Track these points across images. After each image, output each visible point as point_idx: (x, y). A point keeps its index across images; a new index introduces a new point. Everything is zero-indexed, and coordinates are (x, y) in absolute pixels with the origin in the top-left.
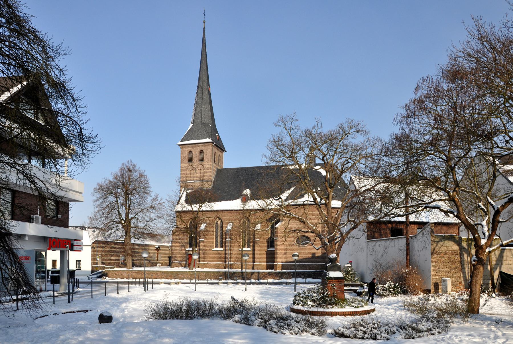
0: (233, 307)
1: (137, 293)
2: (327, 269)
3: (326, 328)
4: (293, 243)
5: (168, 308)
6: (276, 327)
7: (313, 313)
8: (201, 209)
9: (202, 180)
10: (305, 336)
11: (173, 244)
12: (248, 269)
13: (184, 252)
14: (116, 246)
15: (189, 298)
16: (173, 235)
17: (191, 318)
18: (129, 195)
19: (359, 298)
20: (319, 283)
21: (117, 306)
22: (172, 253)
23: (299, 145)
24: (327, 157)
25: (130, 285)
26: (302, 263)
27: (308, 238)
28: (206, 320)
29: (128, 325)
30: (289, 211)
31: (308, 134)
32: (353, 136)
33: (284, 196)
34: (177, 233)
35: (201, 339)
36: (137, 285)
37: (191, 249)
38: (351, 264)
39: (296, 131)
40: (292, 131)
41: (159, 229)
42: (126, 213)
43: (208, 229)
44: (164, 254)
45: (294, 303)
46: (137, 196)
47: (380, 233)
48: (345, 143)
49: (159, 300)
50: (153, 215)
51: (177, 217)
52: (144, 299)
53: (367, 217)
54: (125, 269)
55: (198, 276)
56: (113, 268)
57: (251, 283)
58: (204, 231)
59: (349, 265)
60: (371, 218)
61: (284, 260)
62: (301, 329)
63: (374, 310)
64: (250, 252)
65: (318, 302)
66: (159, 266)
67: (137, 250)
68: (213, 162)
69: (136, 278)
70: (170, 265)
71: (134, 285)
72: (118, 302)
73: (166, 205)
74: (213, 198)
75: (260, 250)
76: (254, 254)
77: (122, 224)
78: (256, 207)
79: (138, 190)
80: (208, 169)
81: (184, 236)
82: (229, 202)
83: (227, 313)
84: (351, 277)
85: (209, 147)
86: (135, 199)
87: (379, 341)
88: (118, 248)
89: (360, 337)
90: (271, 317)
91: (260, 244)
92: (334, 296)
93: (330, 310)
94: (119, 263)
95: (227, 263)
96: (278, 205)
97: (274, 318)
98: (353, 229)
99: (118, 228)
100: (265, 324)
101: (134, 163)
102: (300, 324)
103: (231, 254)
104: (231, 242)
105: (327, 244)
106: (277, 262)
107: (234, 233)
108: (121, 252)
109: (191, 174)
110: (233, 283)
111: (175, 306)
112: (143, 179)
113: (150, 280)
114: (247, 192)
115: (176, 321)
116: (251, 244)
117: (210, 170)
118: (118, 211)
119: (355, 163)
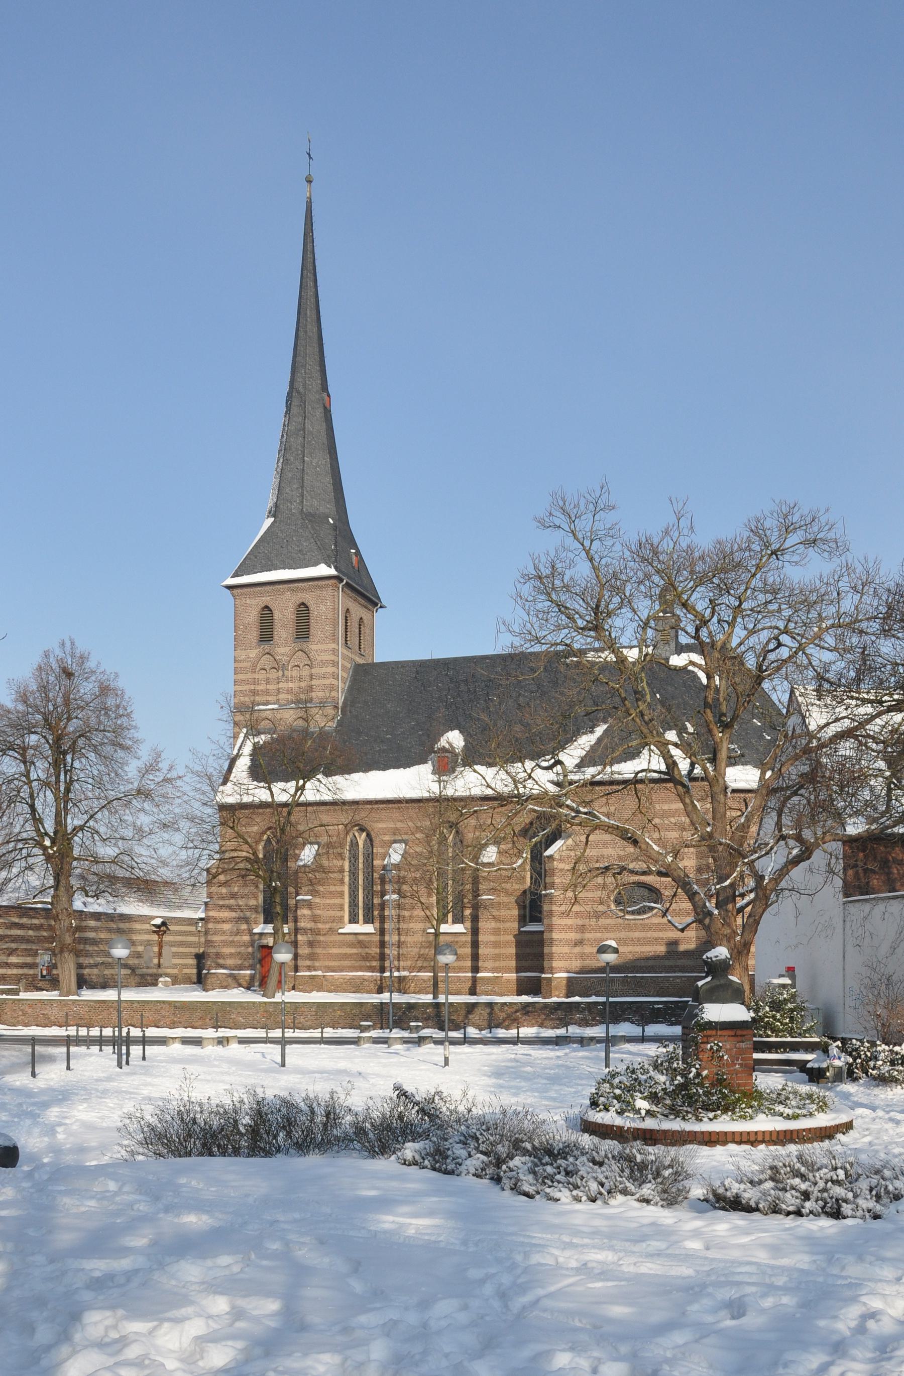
0: (401, 1117)
1: (96, 1076)
2: (700, 997)
3: (686, 1183)
4: (601, 908)
5: (194, 1121)
6: (530, 1178)
7: (650, 1137)
8: (302, 799)
9: (303, 703)
10: (620, 1205)
11: (211, 914)
12: (458, 993)
13: (246, 938)
14: (24, 921)
15: (259, 1091)
16: (209, 883)
17: (268, 1154)
18: (65, 753)
19: (814, 1088)
20: (672, 1039)
21: (34, 1116)
22: (208, 943)
23: (619, 590)
24: (713, 625)
25: (72, 1049)
26: (633, 973)
27: (654, 893)
28: (313, 1160)
29: (66, 1173)
30: (586, 804)
31: (647, 553)
32: (796, 558)
33: (571, 756)
34: (222, 878)
35: (297, 1216)
36: (95, 1049)
37: (269, 929)
38: (793, 977)
39: (608, 542)
40: (596, 544)
41: (164, 863)
42: (58, 814)
43: (325, 863)
44: (181, 944)
45: (594, 1104)
46: (92, 756)
47: (889, 874)
48: (770, 580)
49: (165, 1095)
50: (144, 820)
51: (222, 824)
52: (119, 1092)
53: (843, 825)
54: (53, 995)
55: (293, 1016)
56: (16, 992)
57: (466, 1041)
58: (314, 871)
59: (787, 981)
60: (855, 827)
61: (576, 964)
62: (607, 1186)
63: (848, 1127)
64: (463, 939)
65: (668, 1102)
66: (166, 984)
67: (92, 935)
68: (341, 640)
69: (89, 1026)
70: (201, 980)
71: (83, 1049)
72: (34, 1104)
73: (189, 784)
74: (339, 761)
75: (497, 932)
76: (475, 944)
77: (45, 848)
78: (477, 791)
79: (97, 738)
80: (324, 663)
81: (245, 885)
82: (393, 775)
83: (380, 1137)
84: (792, 1019)
85: (328, 593)
86: (85, 766)
87: (849, 1222)
88: (31, 927)
89: (791, 1209)
90: (517, 1146)
91: (495, 913)
92: (720, 1082)
93: (692, 1126)
94: (34, 976)
95: (387, 974)
96: (552, 782)
97: (526, 1152)
98: (795, 862)
99: (31, 860)
100: (495, 1171)
101: (81, 648)
102: (603, 1169)
103: (399, 944)
104: (399, 906)
105: (710, 914)
106: (552, 970)
107: (410, 875)
108: (40, 940)
109: (268, 681)
110: (406, 1041)
111: (218, 1113)
112: (111, 702)
113: (136, 1032)
114: (455, 739)
115: (218, 1162)
116: (467, 912)
117: (330, 670)
118: (32, 807)
119: (801, 648)
